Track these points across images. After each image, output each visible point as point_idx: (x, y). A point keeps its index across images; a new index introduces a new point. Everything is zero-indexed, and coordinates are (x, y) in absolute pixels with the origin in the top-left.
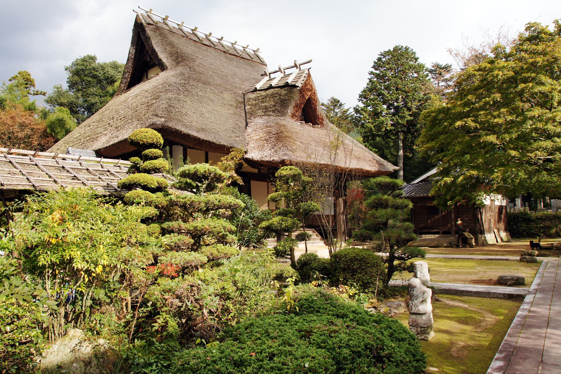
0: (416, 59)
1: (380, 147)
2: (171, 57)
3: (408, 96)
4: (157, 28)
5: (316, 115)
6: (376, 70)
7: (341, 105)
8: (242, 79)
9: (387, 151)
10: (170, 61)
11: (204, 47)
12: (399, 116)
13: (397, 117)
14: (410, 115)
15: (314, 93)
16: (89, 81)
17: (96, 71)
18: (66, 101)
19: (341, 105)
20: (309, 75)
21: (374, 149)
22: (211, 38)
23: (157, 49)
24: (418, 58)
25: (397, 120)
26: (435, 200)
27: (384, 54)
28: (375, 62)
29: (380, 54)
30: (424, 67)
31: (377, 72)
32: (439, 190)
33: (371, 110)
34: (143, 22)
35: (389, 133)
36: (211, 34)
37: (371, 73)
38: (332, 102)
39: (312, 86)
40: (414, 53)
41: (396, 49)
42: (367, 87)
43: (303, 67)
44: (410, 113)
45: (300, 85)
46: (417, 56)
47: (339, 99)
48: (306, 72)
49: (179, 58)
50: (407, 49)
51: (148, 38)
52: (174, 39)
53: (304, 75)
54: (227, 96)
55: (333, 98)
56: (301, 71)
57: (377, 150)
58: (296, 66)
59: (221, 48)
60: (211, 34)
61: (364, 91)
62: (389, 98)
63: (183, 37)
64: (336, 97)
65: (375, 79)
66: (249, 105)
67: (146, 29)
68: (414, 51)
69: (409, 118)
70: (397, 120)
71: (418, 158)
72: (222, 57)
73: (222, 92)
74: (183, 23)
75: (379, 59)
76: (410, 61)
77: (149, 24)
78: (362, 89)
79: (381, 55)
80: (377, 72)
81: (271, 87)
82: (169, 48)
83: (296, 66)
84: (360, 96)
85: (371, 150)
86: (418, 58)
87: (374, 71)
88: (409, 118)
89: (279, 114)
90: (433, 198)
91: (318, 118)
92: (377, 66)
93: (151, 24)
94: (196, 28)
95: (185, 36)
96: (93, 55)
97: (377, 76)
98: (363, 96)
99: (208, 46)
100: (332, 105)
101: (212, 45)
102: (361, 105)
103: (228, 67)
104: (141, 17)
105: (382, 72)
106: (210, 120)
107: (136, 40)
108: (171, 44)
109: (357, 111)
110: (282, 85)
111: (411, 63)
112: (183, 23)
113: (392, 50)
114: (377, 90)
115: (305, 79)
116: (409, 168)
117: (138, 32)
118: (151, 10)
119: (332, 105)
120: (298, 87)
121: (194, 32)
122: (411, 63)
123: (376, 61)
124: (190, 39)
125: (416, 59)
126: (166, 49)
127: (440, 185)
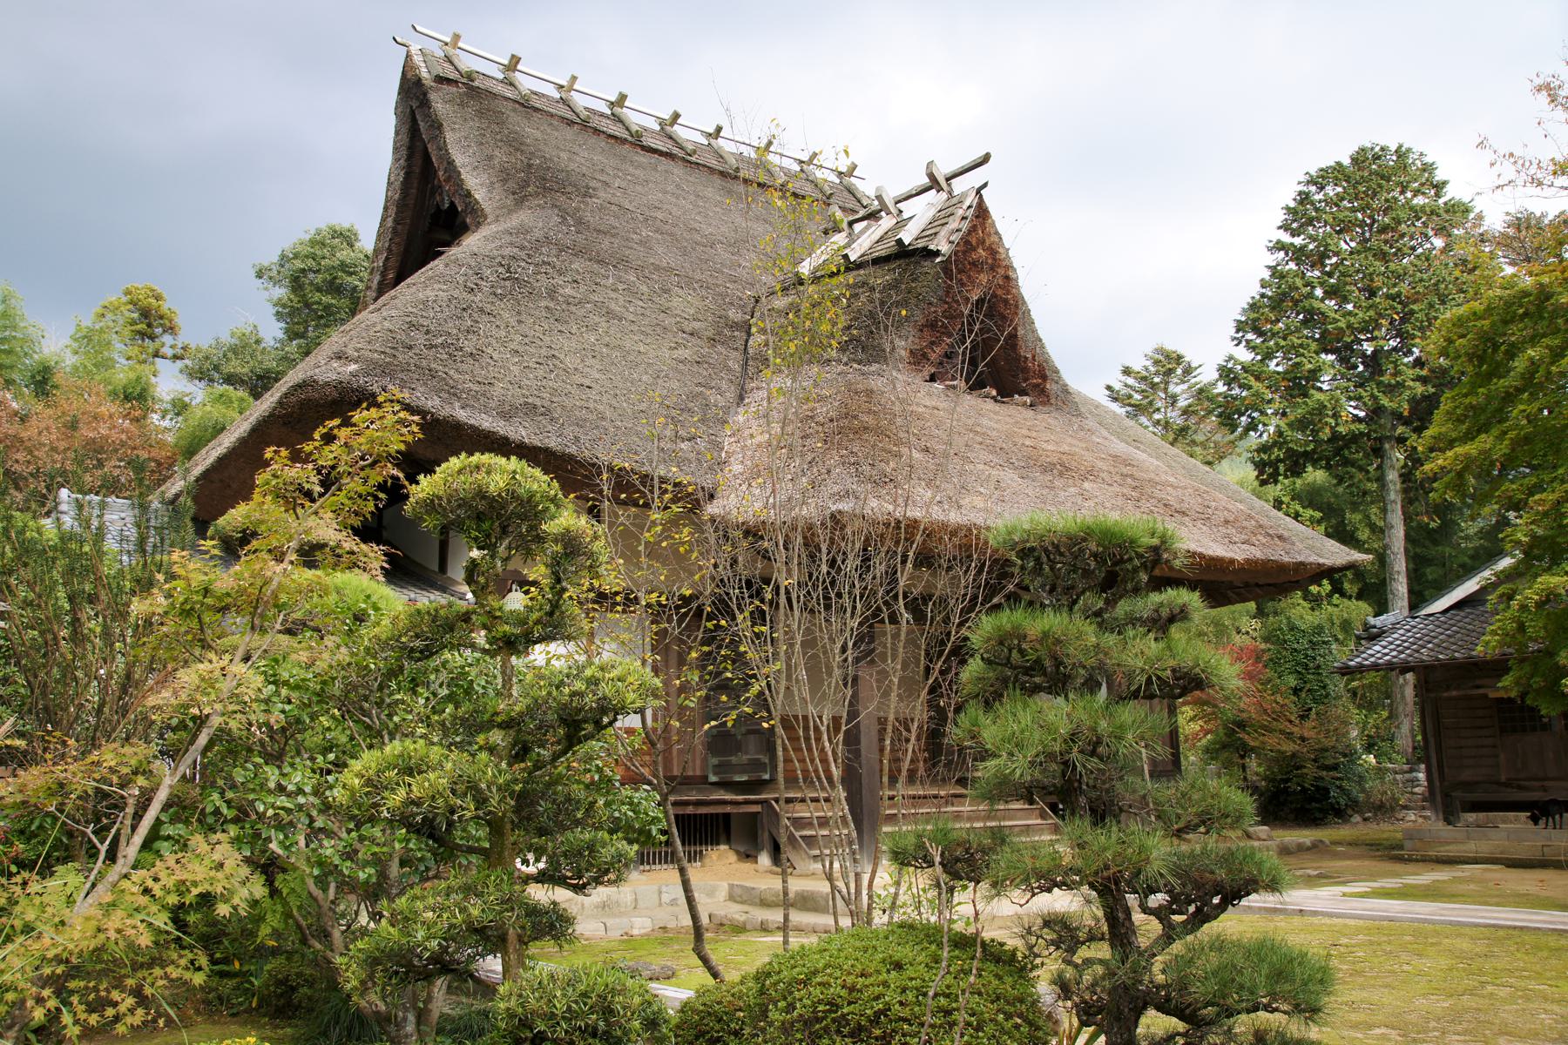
0: (1439, 187)
1: (1329, 505)
2: (504, 181)
3: (1412, 312)
4: (470, 89)
5: (1018, 358)
6: (1293, 236)
7: (1188, 371)
8: (757, 251)
9: (1353, 518)
10: (498, 193)
11: (643, 158)
12: (1379, 384)
13: (1372, 387)
14: (1423, 380)
15: (1007, 278)
16: (327, 307)
17: (351, 274)
18: (246, 370)
19: (1188, 371)
20: (982, 212)
21: (1309, 512)
22: (679, 131)
23: (459, 159)
24: (1445, 183)
25: (1373, 396)
26: (1507, 670)
27: (1320, 180)
28: (1288, 208)
29: (1304, 178)
30: (1467, 211)
31: (1298, 241)
32: (1521, 628)
33: (1280, 369)
34: (424, 73)
35: (1347, 446)
36: (676, 116)
37: (1280, 246)
38: (1157, 362)
39: (993, 252)
40: (1428, 168)
41: (1360, 158)
42: (1263, 296)
43: (959, 185)
44: (1424, 373)
45: (944, 248)
46: (1439, 176)
47: (1181, 351)
48: (971, 199)
49: (532, 181)
50: (1401, 154)
51: (437, 126)
52: (531, 131)
53: (960, 212)
54: (684, 303)
55: (1160, 351)
56: (954, 201)
57: (1318, 515)
58: (934, 184)
59: (713, 163)
60: (676, 116)
61: (1253, 307)
62: (1342, 324)
63: (571, 123)
64: (1170, 347)
65: (1292, 266)
66: (763, 331)
67: (433, 96)
68: (1428, 160)
69: (1419, 389)
70: (1373, 396)
71: (1467, 538)
72: (712, 190)
73: (666, 291)
74: (574, 78)
75: (1304, 198)
76: (1416, 193)
77: (440, 80)
78: (1244, 302)
79: (1311, 182)
80: (1298, 241)
81: (851, 266)
82: (500, 156)
83: (934, 184)
84: (1240, 327)
85: (1296, 516)
86: (1445, 183)
87: (1286, 238)
88: (1419, 389)
89: (860, 355)
90: (1497, 667)
91: (1025, 370)
92: (1300, 215)
93: (449, 81)
94: (623, 98)
95: (583, 124)
96: (346, 225)
97: (1298, 254)
98: (1253, 323)
99: (661, 153)
100: (1157, 373)
101: (676, 151)
102: (1244, 355)
103: (713, 213)
104: (418, 59)
105: (1313, 239)
106: (578, 379)
107: (405, 139)
108: (515, 143)
109: (1226, 374)
110: (883, 253)
111: (1419, 201)
112: (574, 78)
113: (1346, 162)
114: (1296, 302)
115: (965, 226)
116: (1441, 572)
117: (413, 112)
118: (457, 37)
119: (1157, 373)
120: (937, 253)
121: (617, 110)
122: (1419, 201)
123: (1292, 204)
124: (597, 131)
125: (1439, 187)
126: (490, 158)
127: (1523, 608)
